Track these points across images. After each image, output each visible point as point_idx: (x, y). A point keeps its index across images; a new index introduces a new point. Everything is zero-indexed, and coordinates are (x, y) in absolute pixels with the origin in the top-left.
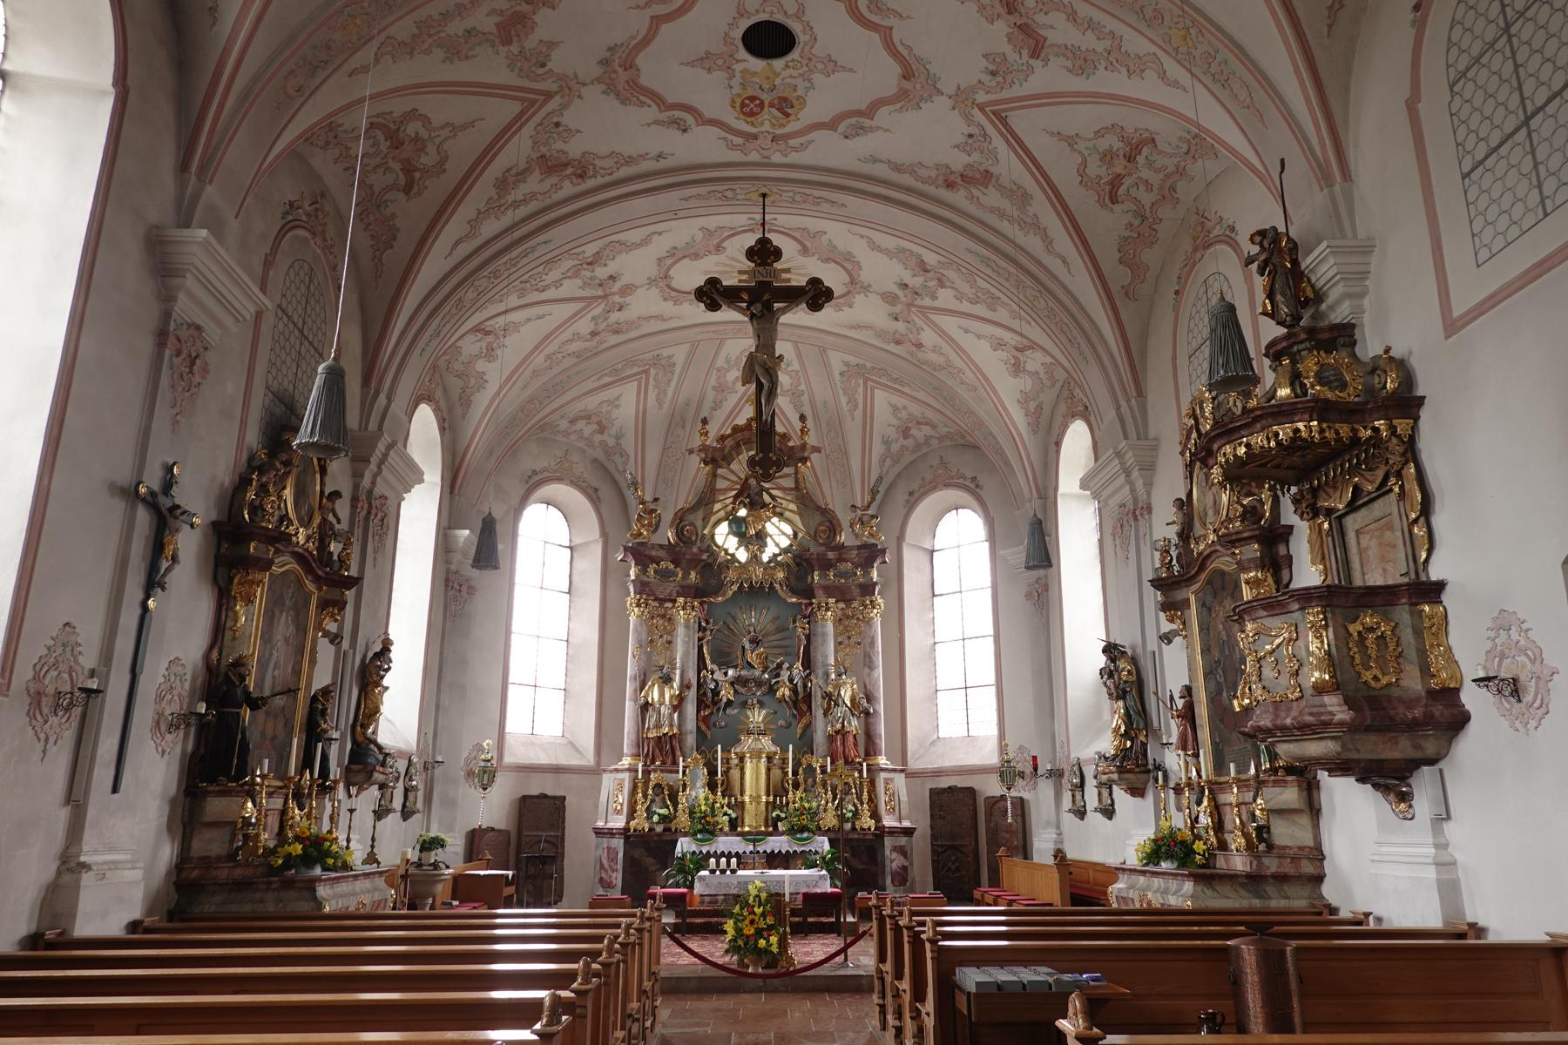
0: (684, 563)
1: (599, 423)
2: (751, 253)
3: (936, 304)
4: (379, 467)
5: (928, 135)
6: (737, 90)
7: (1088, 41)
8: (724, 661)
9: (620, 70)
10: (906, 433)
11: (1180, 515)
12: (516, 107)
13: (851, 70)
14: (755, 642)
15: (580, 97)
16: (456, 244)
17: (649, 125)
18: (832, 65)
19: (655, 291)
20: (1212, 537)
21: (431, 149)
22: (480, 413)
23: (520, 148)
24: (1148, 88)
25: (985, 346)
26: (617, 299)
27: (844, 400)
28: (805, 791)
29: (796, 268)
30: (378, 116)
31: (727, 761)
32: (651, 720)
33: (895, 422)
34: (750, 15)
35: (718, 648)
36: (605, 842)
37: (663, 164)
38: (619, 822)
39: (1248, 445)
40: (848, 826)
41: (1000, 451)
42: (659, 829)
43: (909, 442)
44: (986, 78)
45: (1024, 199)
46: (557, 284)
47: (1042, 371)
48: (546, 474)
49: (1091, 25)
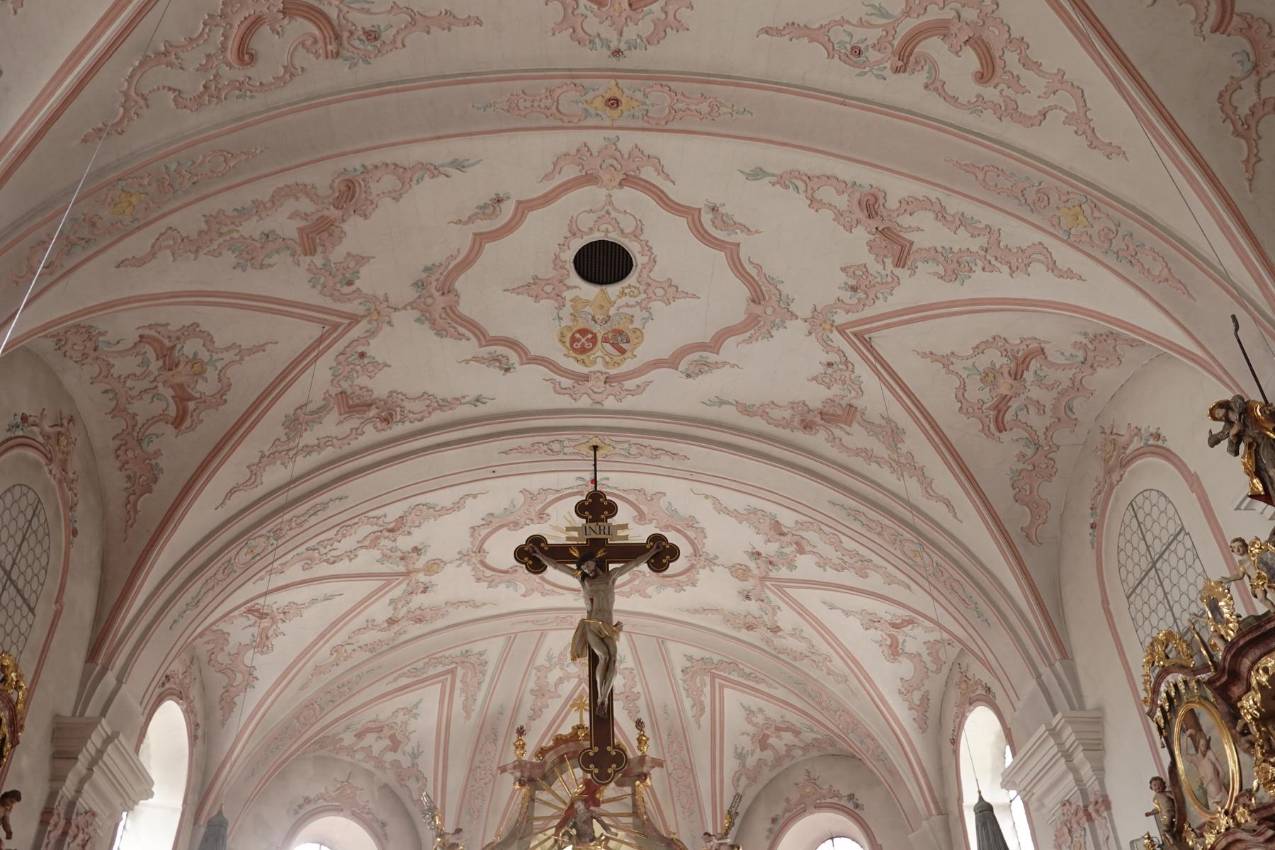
1: (392, 737)
2: (580, 509)
3: (795, 575)
4: (90, 769)
5: (781, 369)
6: (567, 322)
7: (962, 240)
9: (437, 294)
10: (763, 743)
11: (1163, 800)
12: (315, 331)
13: (694, 296)
15: (389, 323)
16: (232, 492)
17: (467, 362)
18: (672, 291)
19: (466, 568)
20: (1224, 821)
21: (211, 374)
22: (244, 720)
23: (317, 381)
24: (1037, 284)
25: (854, 624)
26: (422, 577)
27: (687, 703)
29: (631, 527)
30: (150, 327)
33: (751, 729)
34: (583, 234)
37: (481, 410)
39: (1266, 670)
41: (882, 758)
43: (768, 755)
44: (846, 295)
45: (893, 434)
46: (351, 555)
47: (924, 651)
48: (321, 803)
49: (964, 222)
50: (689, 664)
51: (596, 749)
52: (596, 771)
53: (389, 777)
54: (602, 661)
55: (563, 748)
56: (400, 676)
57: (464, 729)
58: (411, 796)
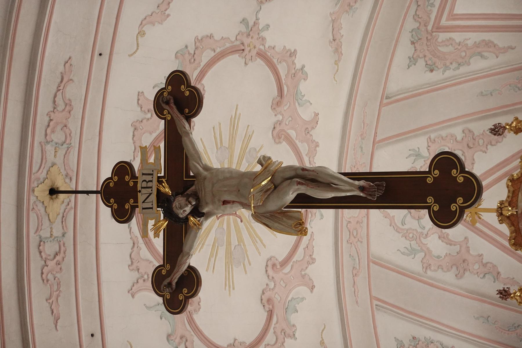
2: (122, 216)
27: (478, 64)
50: (421, 63)
51: (430, 200)
52: (460, 200)
54: (303, 190)
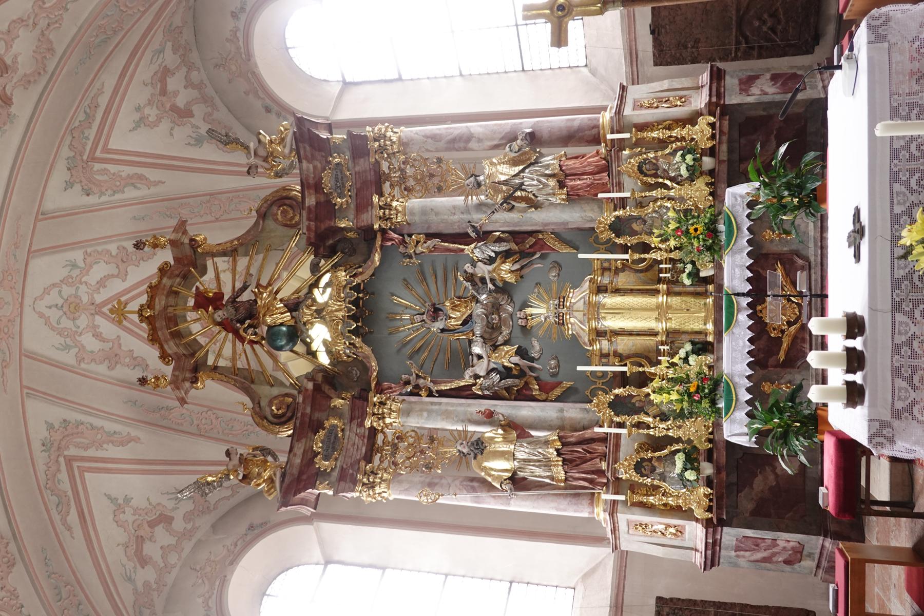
0: (317, 415)
1: (152, 524)
8: (463, 359)
14: (436, 312)
27: (131, 193)
28: (651, 233)
31: (604, 357)
32: (535, 473)
33: (165, 125)
35: (442, 371)
36: (726, 554)
38: (696, 533)
40: (708, 162)
42: (708, 469)
43: (199, 110)
48: (212, 603)
50: (77, 187)
53: (204, 523)
55: (163, 334)
56: (64, 522)
57: (150, 444)
58: (227, 498)
